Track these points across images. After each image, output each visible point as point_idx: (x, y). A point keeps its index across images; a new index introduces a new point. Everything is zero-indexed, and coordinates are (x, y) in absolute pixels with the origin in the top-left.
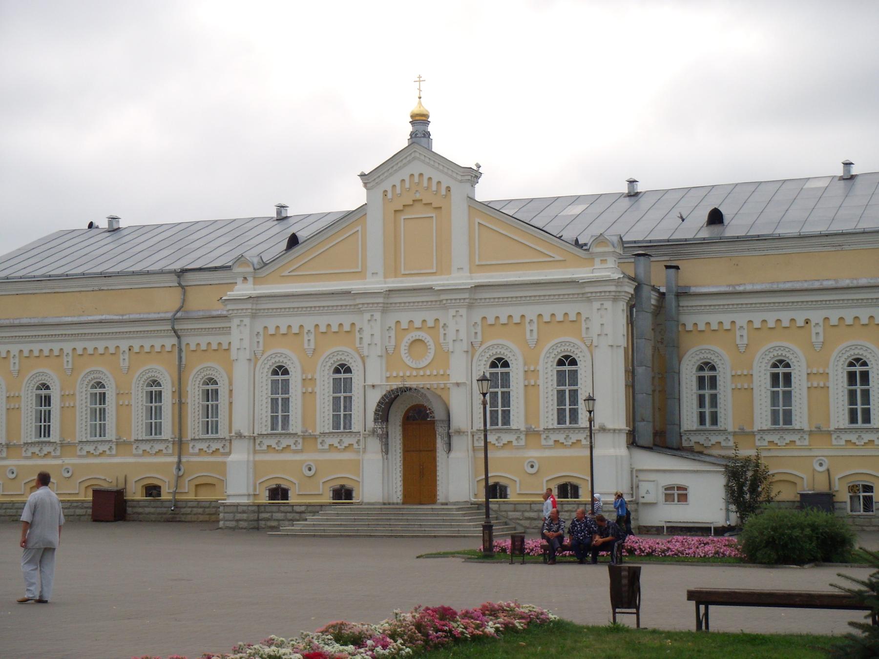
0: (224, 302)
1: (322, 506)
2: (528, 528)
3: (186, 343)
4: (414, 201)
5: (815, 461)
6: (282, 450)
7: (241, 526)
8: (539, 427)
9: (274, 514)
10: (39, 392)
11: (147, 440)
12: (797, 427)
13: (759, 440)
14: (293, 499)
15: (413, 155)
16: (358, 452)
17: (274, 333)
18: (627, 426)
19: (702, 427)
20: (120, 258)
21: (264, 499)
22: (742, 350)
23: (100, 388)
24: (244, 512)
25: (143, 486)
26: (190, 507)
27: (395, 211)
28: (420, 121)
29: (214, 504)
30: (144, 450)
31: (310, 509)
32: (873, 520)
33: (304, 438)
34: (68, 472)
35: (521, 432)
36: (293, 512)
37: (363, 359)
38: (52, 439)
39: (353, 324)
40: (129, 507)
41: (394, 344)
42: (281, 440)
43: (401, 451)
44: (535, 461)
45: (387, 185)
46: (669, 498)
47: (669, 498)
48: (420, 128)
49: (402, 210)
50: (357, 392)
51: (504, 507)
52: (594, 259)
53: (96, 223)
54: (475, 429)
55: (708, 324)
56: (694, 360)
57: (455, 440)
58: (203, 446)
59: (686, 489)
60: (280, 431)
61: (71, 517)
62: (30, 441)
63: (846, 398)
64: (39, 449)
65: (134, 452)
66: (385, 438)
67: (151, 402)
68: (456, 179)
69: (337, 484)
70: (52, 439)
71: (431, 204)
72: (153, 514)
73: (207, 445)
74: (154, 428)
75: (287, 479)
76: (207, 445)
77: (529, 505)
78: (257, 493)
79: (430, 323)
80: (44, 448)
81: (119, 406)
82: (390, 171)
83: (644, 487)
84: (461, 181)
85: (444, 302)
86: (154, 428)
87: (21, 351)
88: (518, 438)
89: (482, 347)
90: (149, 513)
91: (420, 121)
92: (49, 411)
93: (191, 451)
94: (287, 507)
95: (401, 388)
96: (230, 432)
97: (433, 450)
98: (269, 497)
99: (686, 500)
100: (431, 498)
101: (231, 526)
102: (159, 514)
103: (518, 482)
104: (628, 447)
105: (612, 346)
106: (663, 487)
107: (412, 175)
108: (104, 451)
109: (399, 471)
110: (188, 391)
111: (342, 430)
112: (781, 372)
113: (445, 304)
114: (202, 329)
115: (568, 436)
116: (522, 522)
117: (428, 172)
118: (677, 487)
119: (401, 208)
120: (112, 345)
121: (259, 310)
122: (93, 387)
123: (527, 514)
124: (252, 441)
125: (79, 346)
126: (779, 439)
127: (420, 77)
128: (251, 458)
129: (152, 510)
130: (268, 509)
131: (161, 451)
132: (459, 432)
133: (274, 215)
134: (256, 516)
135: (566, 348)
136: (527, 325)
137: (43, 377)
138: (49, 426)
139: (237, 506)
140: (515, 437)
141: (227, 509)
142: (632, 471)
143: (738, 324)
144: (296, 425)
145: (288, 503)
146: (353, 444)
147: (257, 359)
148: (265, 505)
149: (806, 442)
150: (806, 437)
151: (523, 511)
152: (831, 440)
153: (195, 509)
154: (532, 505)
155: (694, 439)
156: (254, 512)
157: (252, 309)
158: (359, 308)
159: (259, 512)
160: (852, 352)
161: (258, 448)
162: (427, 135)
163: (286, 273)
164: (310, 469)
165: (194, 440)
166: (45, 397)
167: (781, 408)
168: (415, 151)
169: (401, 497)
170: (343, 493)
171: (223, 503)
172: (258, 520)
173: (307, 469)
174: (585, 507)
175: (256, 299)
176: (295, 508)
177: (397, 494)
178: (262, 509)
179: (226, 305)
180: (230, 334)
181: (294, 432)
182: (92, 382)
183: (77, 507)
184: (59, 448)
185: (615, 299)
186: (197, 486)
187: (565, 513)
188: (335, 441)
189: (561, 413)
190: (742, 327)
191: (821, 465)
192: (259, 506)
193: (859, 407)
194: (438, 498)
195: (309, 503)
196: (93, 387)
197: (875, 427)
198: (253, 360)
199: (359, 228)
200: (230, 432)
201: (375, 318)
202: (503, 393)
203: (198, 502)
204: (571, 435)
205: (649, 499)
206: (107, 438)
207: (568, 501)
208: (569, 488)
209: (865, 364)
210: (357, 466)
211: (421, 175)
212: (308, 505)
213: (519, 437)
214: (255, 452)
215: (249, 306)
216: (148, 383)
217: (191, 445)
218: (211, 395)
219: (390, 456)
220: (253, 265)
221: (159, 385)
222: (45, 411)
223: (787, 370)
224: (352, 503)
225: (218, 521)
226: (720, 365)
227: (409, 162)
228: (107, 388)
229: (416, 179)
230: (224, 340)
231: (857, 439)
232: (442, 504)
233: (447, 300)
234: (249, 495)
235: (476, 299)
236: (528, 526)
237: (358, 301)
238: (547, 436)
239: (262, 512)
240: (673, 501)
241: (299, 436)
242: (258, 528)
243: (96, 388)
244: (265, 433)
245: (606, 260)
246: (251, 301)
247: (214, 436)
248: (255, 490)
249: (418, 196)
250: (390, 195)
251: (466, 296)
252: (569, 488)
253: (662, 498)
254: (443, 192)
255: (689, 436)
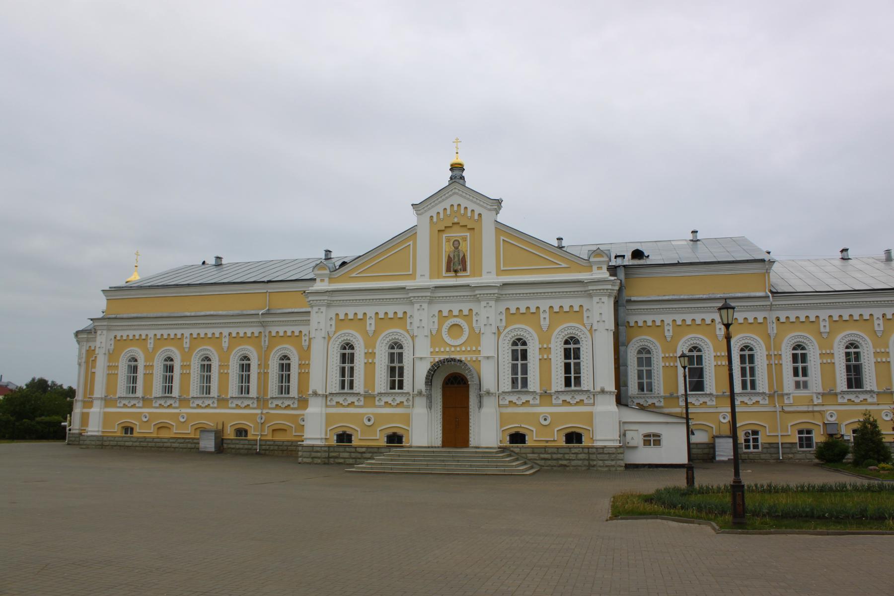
0: (307, 295)
1: (379, 448)
2: (543, 466)
3: (269, 331)
4: (453, 224)
5: (720, 416)
6: (347, 406)
7: (315, 462)
8: (551, 390)
9: (341, 454)
10: (166, 363)
11: (239, 398)
12: (868, 389)
13: (555, 399)
14: (355, 442)
15: (453, 191)
16: (408, 407)
17: (352, 318)
18: (616, 389)
19: (568, 389)
20: (225, 276)
21: (333, 441)
22: (187, 350)
23: (208, 361)
24: (317, 452)
25: (235, 429)
26: (268, 445)
27: (439, 231)
28: (457, 169)
29: (294, 444)
30: (337, 402)
31: (370, 450)
32: (762, 455)
33: (365, 397)
34: (183, 418)
35: (590, 393)
36: (356, 452)
37: (413, 337)
38: (173, 395)
39: (405, 313)
40: (225, 444)
41: (437, 327)
42: (348, 398)
43: (441, 407)
44: (371, 416)
45: (433, 212)
46: (647, 443)
47: (647, 443)
48: (457, 173)
49: (451, 227)
50: (407, 363)
51: (523, 451)
52: (592, 266)
53: (207, 262)
54: (500, 391)
55: (645, 322)
56: (636, 346)
57: (486, 401)
58: (279, 402)
59: (659, 436)
60: (346, 390)
61: (185, 450)
62: (122, 396)
63: (757, 373)
64: (164, 401)
65: (230, 405)
66: (429, 398)
67: (243, 371)
68: (485, 208)
69: (390, 432)
70: (173, 395)
71: (466, 226)
72: (242, 449)
73: (281, 402)
74: (244, 390)
75: (351, 426)
76: (281, 402)
77: (544, 449)
78: (328, 437)
79: (466, 312)
80: (168, 401)
81: (220, 374)
82: (429, 206)
83: (629, 435)
84: (490, 210)
85: (478, 296)
86: (244, 390)
87: (155, 335)
88: (213, 403)
89: (506, 330)
90: (239, 449)
91: (457, 169)
92: (172, 376)
93: (270, 406)
94: (351, 449)
95: (447, 359)
96: (326, 392)
97: (467, 407)
98: (566, 441)
99: (660, 445)
100: (465, 443)
101: (307, 461)
102: (246, 449)
103: (535, 432)
104: (617, 405)
105: (607, 330)
106: (642, 435)
107: (452, 205)
108: (209, 405)
109: (439, 423)
110: (269, 365)
111: (645, 392)
112: (695, 355)
113: (478, 297)
114: (281, 321)
115: (203, 402)
116: (538, 462)
117: (464, 203)
118: (653, 435)
119: (444, 229)
120: (217, 332)
121: (333, 301)
122: (203, 360)
123: (542, 456)
124: (324, 398)
125: (195, 332)
126: (517, 399)
127: (457, 139)
128: (324, 412)
129: (241, 446)
130: (336, 449)
131: (289, 405)
132: (488, 393)
133: (323, 257)
134: (327, 455)
135: (571, 331)
136: (474, 317)
137: (169, 353)
138: (172, 386)
139: (313, 446)
140: (532, 397)
141: (305, 449)
142: (620, 423)
143: (666, 323)
144: (359, 387)
145: (351, 445)
146: (403, 402)
147: (330, 338)
148: (333, 447)
149: (714, 403)
150: (714, 399)
151: (539, 453)
152: (784, 400)
153: (272, 447)
154: (546, 449)
155: (636, 401)
156: (325, 451)
157: (328, 300)
158: (411, 301)
159: (329, 452)
160: (743, 342)
161: (329, 403)
162: (462, 178)
163: (353, 275)
164: (369, 420)
165: (272, 398)
166: (170, 366)
167: (397, 379)
168: (455, 188)
169: (441, 443)
170: (395, 439)
171: (301, 444)
172: (329, 457)
173: (367, 420)
174: (603, 450)
175: (331, 293)
176: (358, 449)
177: (438, 442)
178: (332, 449)
179: (308, 297)
180: (309, 325)
181: (357, 392)
182: (202, 357)
183: (188, 442)
184: (178, 402)
185: (609, 296)
186: (274, 430)
187: (572, 455)
188: (389, 399)
189: (514, 381)
190: (668, 324)
191: (831, 416)
192: (329, 447)
193: (645, 381)
194: (470, 443)
195: (368, 445)
196: (203, 360)
197: (760, 392)
198: (328, 338)
199: (411, 243)
200: (326, 392)
201: (423, 307)
202: (575, 363)
203: (274, 441)
204: (205, 401)
205: (632, 443)
206: (211, 395)
207: (574, 446)
208: (574, 436)
209: (751, 349)
210: (407, 419)
211: (459, 205)
212: (368, 447)
213: (253, 402)
214: (327, 406)
215: (326, 298)
216: (241, 359)
217: (270, 402)
218: (285, 367)
219: (433, 410)
220: (329, 269)
221: (249, 359)
222: (169, 376)
223: (287, 362)
224: (402, 446)
225: (298, 457)
226: (654, 350)
227: (451, 196)
228: (212, 361)
229: (455, 208)
230: (305, 330)
231: (392, 401)
232: (473, 447)
233: (480, 294)
234: (322, 439)
235: (502, 295)
236: (543, 464)
237: (411, 295)
238: (519, 397)
239: (332, 452)
240: (650, 445)
241: (361, 395)
242: (328, 464)
243: (205, 361)
244: (335, 392)
245: (601, 267)
246: (328, 294)
247: (287, 396)
248: (326, 434)
249: (456, 220)
250: (435, 219)
251: (496, 291)
252: (574, 436)
253: (642, 443)
254: (476, 217)
255: (751, 397)
